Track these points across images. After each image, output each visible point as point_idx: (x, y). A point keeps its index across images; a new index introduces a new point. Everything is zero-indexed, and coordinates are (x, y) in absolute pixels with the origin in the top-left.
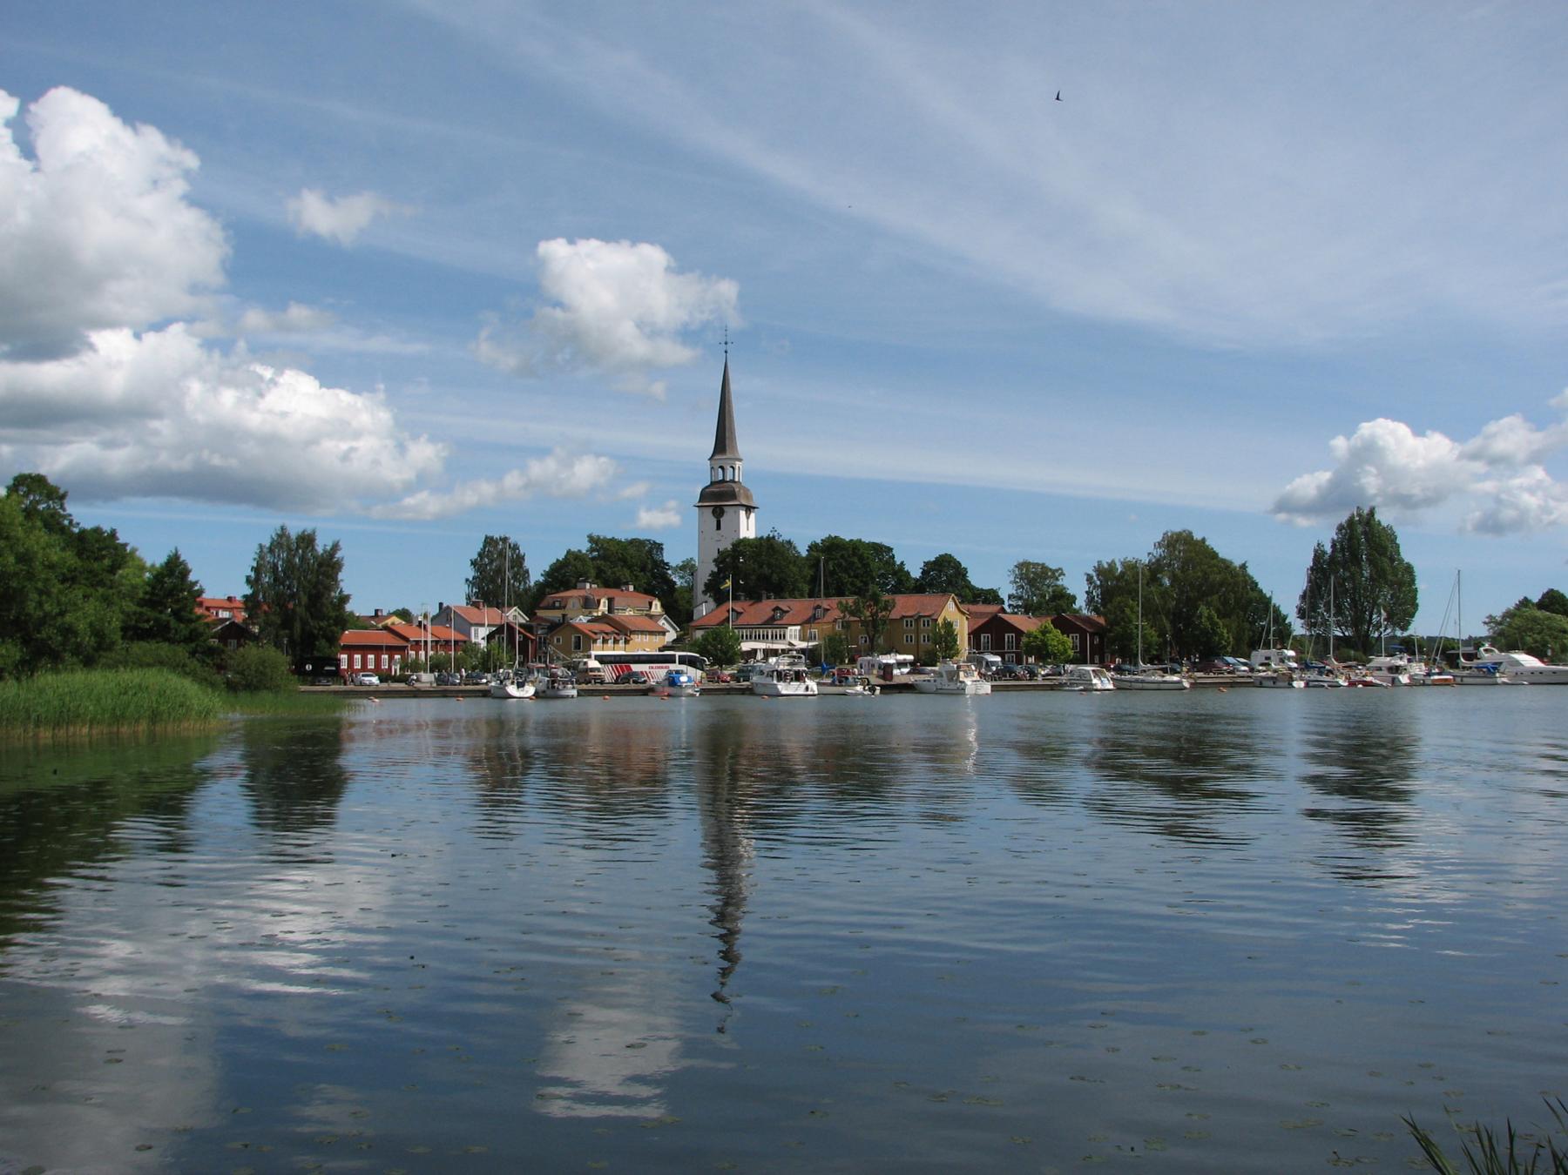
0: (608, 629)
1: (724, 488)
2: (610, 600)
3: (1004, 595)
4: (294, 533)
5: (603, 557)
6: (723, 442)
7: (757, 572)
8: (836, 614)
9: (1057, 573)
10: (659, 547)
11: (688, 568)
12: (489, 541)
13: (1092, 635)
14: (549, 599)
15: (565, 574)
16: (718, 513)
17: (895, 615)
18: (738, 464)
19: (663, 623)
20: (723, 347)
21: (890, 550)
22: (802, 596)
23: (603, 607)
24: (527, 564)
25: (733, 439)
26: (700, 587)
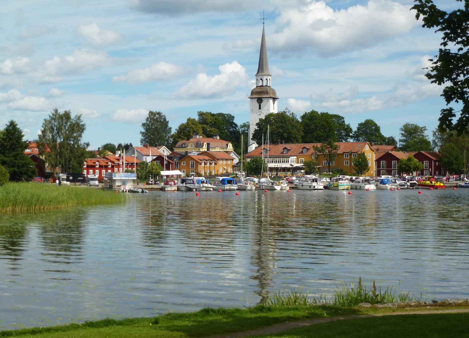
0: (207, 158)
2: (208, 144)
3: (397, 139)
4: (61, 112)
7: (279, 130)
8: (312, 151)
9: (423, 129)
10: (233, 117)
11: (246, 126)
12: (151, 113)
13: (435, 161)
14: (180, 143)
15: (186, 132)
16: (260, 101)
17: (340, 152)
18: (269, 78)
19: (233, 155)
20: (262, 21)
21: (343, 118)
22: (298, 142)
23: (204, 149)
24: (170, 125)
25: (267, 65)
26: (251, 136)
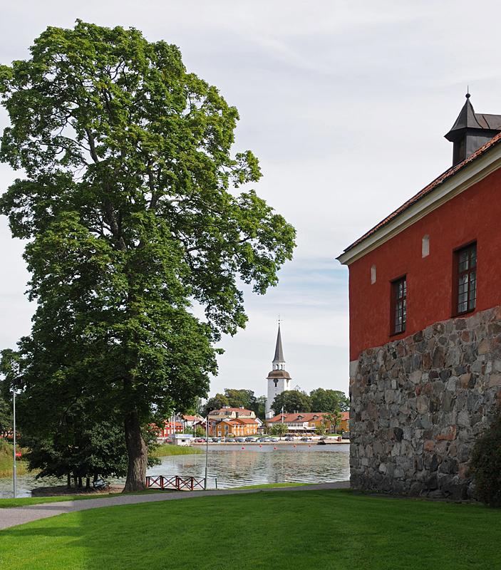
1: (278, 372)
2: (237, 413)
5: (231, 396)
6: (278, 356)
7: (291, 403)
16: (276, 381)
25: (282, 353)
